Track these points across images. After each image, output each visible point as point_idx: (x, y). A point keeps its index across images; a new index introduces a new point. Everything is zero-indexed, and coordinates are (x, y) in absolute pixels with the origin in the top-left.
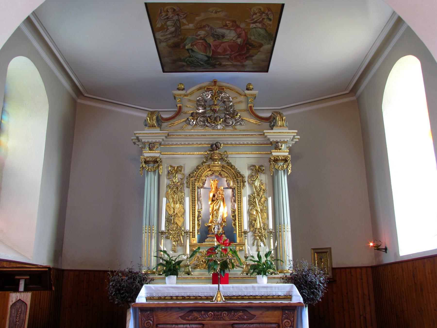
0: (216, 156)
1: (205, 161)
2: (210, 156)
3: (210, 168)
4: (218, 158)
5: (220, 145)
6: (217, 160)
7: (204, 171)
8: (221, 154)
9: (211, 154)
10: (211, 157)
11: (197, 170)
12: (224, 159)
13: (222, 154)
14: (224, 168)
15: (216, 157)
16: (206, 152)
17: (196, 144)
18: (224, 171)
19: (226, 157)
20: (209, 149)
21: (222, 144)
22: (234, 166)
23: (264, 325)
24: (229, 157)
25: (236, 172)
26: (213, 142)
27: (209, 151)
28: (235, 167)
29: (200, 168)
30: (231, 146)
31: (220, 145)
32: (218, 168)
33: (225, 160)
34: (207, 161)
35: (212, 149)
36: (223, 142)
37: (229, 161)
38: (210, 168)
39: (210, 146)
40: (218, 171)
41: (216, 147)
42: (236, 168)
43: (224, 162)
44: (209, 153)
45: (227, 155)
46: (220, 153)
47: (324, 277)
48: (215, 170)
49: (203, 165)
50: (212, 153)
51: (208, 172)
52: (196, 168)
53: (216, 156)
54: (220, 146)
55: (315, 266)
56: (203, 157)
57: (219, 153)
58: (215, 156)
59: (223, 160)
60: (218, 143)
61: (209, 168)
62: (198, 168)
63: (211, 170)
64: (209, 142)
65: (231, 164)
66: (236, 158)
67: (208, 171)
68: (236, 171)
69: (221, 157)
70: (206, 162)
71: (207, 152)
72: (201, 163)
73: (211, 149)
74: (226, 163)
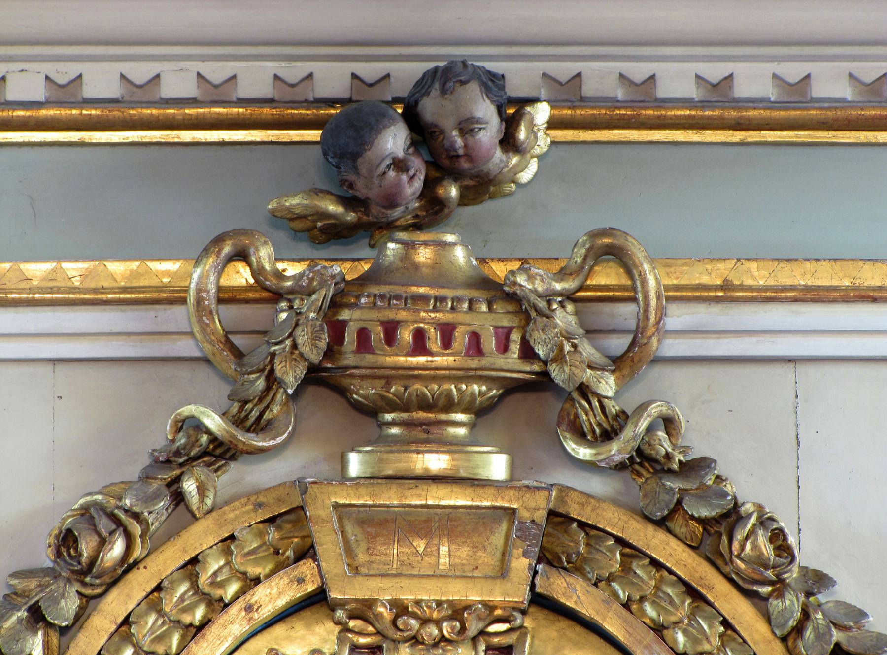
0: (434, 341)
1: (214, 422)
2: (302, 338)
3: (307, 552)
4: (467, 375)
5: (510, 124)
6: (450, 406)
7: (206, 623)
8: (513, 298)
9: (336, 304)
10: (330, 353)
11: (70, 604)
12: (584, 390)
13: (548, 296)
14: (576, 568)
15: (420, 345)
16: (242, 255)
17: (39, 93)
18: (588, 610)
19: (619, 344)
20: (294, 202)
21: (542, 113)
22: (765, 521)
23: (723, 103)
24: (673, 347)
25: (799, 630)
26: (369, 70)
27: (296, 234)
28: (778, 538)
29: (127, 566)
30: (710, 136)
31: (510, 124)
32: (464, 552)
33: (589, 419)
34: (260, 426)
35: (350, 202)
36: (564, 70)
37: (669, 423)
38: (306, 567)
39: (314, 135)
40: (458, 612)
41: (417, 165)
42: (802, 559)
43: (584, 453)
44: (292, 269)
45: (627, 313)
46: (499, 270)
47: (372, 390)
48: (400, 609)
49: (179, 498)
50: (350, 271)
51: (279, 630)
52: (45, 559)
53: (434, 341)
54: (509, 142)
55: (312, 353)
56: (186, 347)
57: (486, 284)
58: (406, 336)
59: (554, 406)
60: (474, 89)
61: (299, 557)
62: (86, 547)
63: (335, 595)
64: (294, 71)
65: (705, 494)
66: (802, 369)
67: (266, 612)
68: (806, 615)
69: (527, 352)
70: (241, 436)
71: (264, 254)
72: (133, 472)
73: (333, 208)
74: (621, 467)
